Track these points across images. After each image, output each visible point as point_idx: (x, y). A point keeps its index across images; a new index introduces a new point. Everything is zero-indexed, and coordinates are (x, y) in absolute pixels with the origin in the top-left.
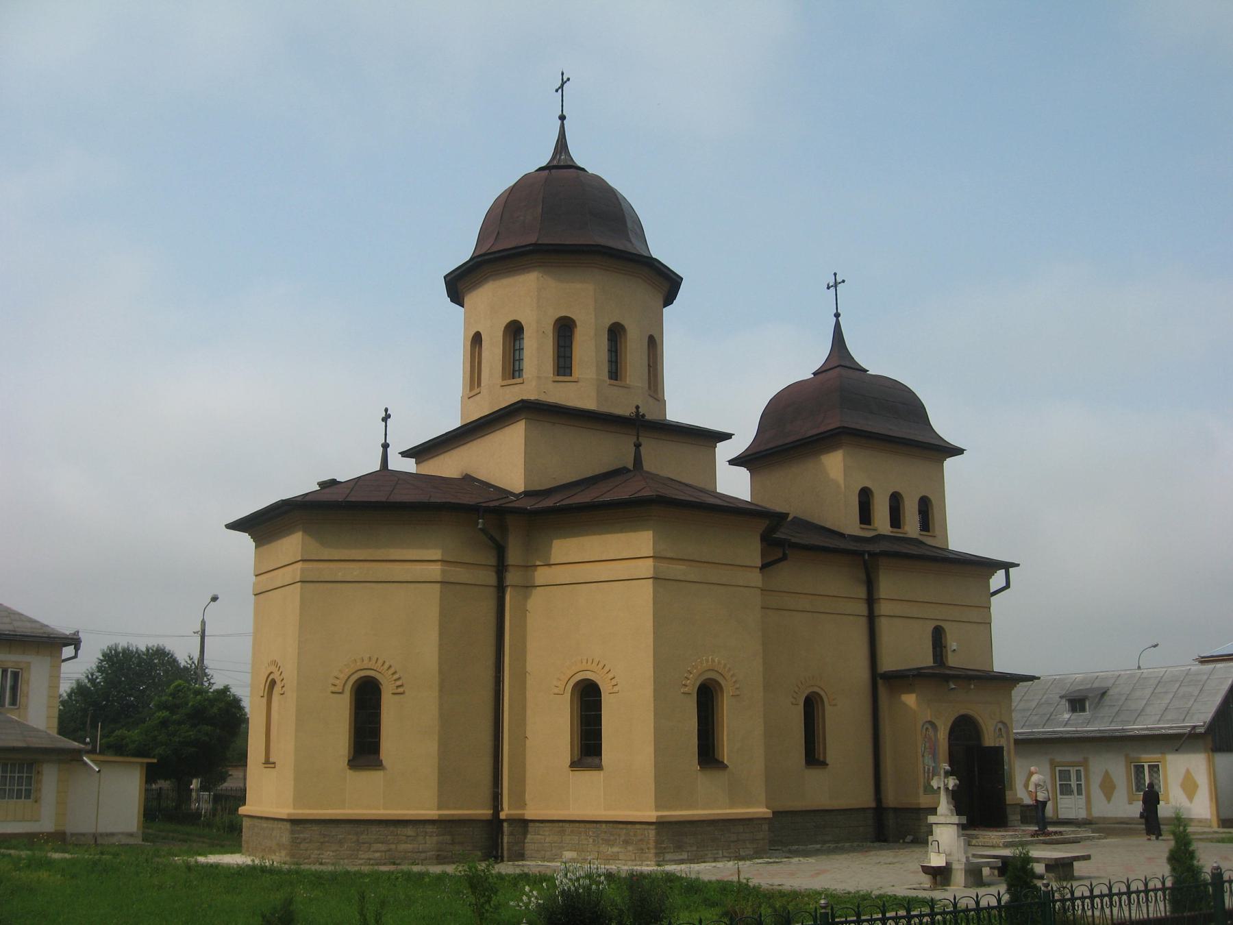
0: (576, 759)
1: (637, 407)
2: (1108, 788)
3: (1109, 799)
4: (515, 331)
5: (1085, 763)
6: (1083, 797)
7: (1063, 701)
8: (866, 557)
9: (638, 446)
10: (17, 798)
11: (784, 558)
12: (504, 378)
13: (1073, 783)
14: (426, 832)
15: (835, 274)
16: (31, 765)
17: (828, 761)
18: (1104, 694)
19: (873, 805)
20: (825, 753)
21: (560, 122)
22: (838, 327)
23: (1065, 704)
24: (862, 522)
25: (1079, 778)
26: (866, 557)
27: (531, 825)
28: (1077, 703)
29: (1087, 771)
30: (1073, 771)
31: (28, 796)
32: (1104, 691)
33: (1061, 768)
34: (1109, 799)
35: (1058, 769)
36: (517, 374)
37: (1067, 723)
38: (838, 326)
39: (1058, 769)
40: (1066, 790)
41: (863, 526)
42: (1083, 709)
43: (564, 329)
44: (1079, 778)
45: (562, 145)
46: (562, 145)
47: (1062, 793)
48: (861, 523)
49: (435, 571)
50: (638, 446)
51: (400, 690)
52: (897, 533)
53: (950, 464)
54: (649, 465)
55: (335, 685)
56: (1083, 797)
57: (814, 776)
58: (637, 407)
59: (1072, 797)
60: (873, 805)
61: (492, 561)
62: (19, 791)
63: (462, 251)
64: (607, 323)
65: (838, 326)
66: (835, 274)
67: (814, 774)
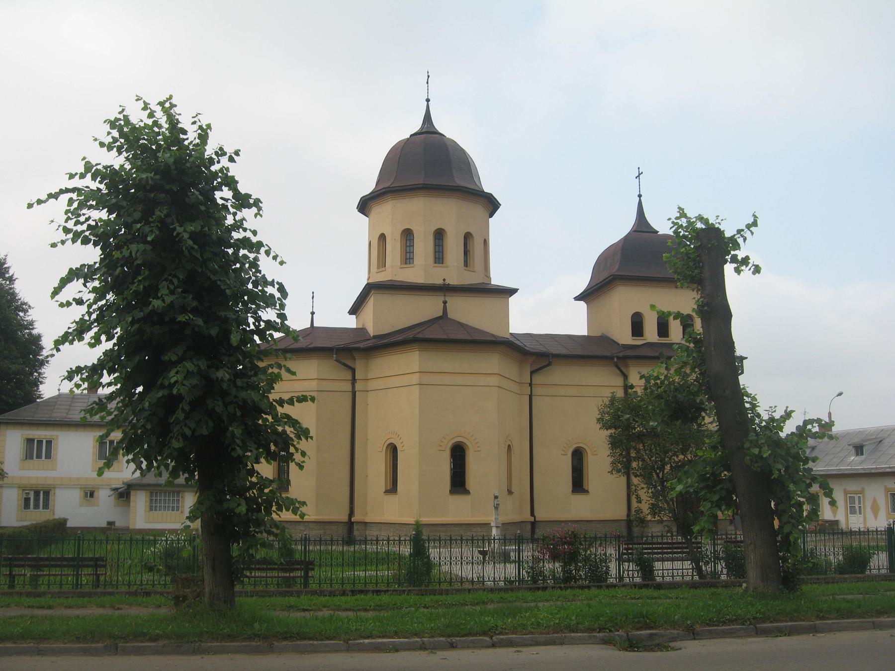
0: (389, 488)
1: (444, 280)
2: (875, 510)
3: (876, 517)
4: (408, 234)
5: (862, 492)
6: (862, 515)
7: (851, 447)
8: (615, 360)
9: (445, 303)
10: (177, 510)
11: (549, 364)
12: (401, 264)
13: (857, 506)
14: (309, 528)
15: (639, 168)
16: (178, 493)
17: (513, 491)
18: (880, 441)
19: (625, 518)
20: (588, 488)
21: (426, 103)
22: (640, 204)
23: (853, 451)
24: (633, 335)
25: (860, 503)
26: (615, 360)
27: (368, 524)
28: (859, 449)
29: (863, 497)
30: (856, 497)
31: (178, 510)
32: (879, 440)
33: (851, 495)
34: (876, 517)
35: (848, 495)
36: (408, 261)
37: (854, 462)
38: (640, 204)
39: (848, 495)
40: (853, 511)
41: (634, 338)
42: (862, 454)
43: (439, 235)
44: (860, 503)
45: (428, 118)
46: (428, 118)
47: (851, 513)
48: (633, 336)
49: (415, 379)
50: (445, 303)
51: (479, 449)
52: (664, 340)
53: (512, 300)
54: (451, 315)
55: (441, 446)
56: (862, 515)
57: (579, 499)
58: (444, 280)
59: (856, 515)
60: (625, 518)
61: (350, 377)
62: (173, 507)
63: (369, 186)
64: (433, 228)
65: (640, 204)
66: (639, 168)
67: (579, 498)
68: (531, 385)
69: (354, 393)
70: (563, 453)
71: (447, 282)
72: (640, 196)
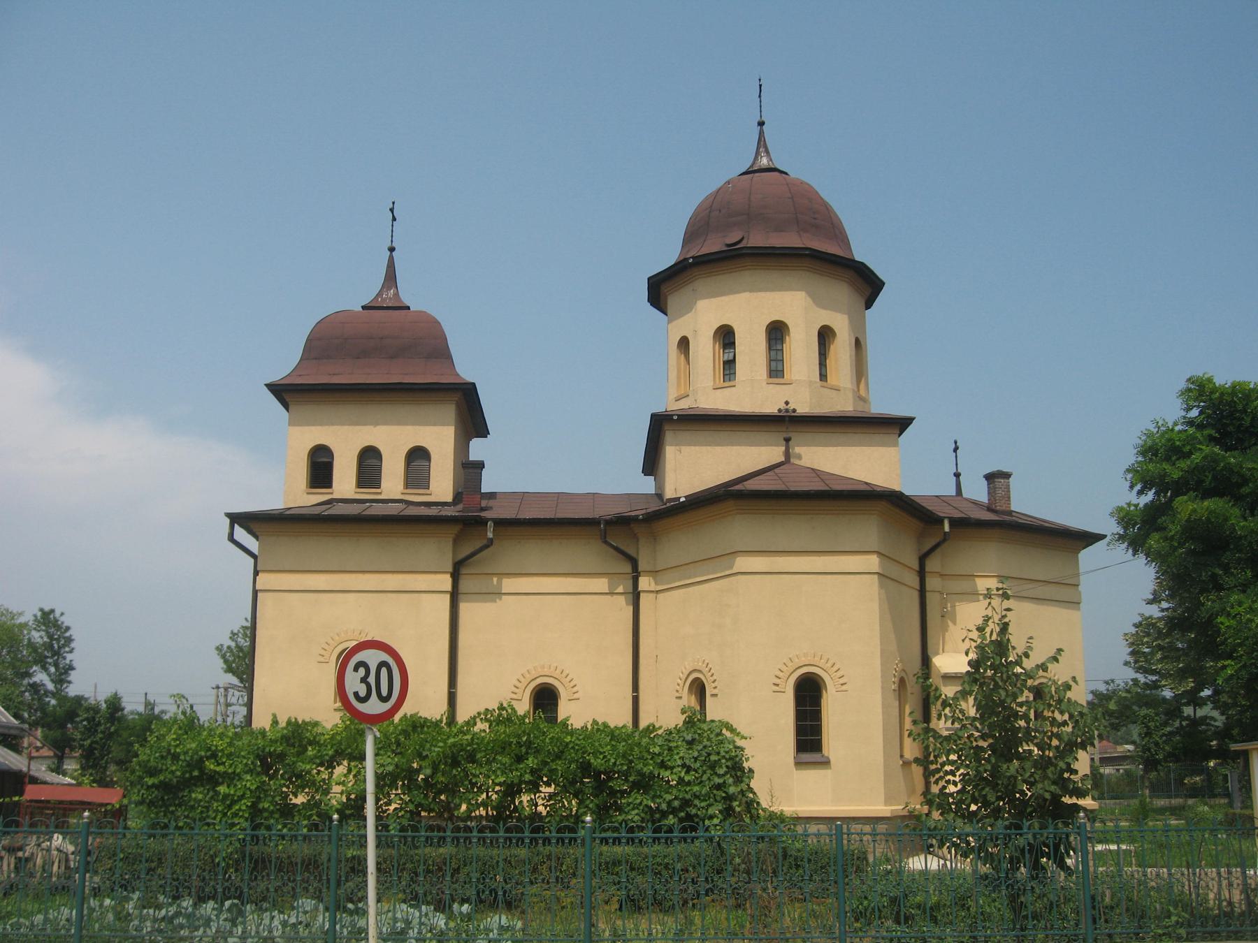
1: (787, 403)
52: (366, 494)
68: (922, 573)
70: (322, 659)
71: (791, 406)
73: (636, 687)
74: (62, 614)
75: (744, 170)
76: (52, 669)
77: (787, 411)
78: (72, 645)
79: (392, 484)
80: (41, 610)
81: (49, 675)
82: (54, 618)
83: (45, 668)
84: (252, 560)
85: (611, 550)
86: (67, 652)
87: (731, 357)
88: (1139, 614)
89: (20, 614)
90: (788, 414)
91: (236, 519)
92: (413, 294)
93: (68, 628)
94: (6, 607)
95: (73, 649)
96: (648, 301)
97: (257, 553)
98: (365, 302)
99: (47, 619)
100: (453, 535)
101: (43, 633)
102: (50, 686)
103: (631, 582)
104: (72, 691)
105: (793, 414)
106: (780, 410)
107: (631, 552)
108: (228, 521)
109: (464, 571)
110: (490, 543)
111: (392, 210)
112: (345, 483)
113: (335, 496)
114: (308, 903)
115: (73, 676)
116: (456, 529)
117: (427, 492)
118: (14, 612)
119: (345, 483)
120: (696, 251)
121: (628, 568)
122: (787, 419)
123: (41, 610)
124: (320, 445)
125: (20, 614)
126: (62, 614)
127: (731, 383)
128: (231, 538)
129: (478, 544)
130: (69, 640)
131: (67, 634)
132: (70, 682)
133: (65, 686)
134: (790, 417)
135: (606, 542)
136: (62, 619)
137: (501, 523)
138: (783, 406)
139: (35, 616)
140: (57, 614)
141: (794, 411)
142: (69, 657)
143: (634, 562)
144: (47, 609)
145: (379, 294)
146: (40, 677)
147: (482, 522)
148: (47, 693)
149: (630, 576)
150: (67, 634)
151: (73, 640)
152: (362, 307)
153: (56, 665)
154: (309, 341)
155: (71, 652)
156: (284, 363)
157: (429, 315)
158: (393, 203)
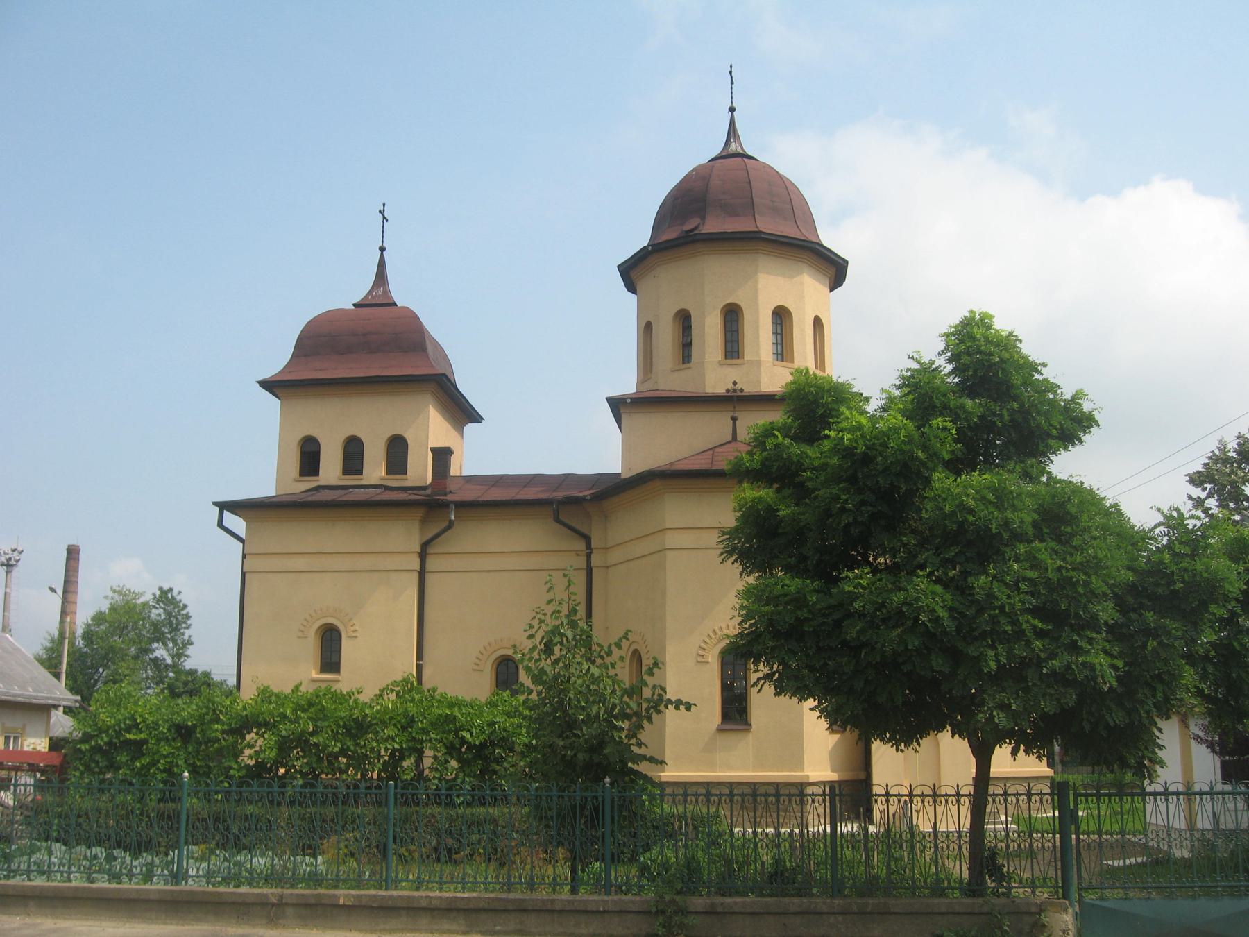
1: (735, 383)
9: (734, 419)
36: (686, 359)
43: (684, 320)
50: (734, 419)
52: (394, 482)
69: (589, 571)
71: (739, 386)
72: (382, 249)
73: (420, 656)
74: (180, 593)
75: (713, 156)
76: (171, 645)
77: (735, 391)
78: (189, 622)
79: (375, 470)
80: (160, 589)
81: (168, 650)
82: (172, 596)
83: (165, 645)
84: (241, 545)
85: (566, 530)
86: (185, 628)
87: (689, 341)
88: (145, 592)
89: (142, 594)
90: (736, 394)
91: (223, 506)
92: (401, 294)
93: (185, 606)
94: (128, 587)
95: (190, 625)
96: (629, 290)
97: (244, 538)
98: (357, 299)
99: (165, 597)
100: (419, 518)
101: (161, 611)
102: (169, 661)
103: (585, 558)
104: (189, 664)
105: (740, 394)
106: (728, 391)
107: (584, 530)
108: (217, 509)
109: (430, 550)
110: (450, 526)
111: (382, 212)
112: (331, 470)
113: (322, 483)
114: (145, 855)
115: (190, 650)
116: (421, 512)
117: (404, 477)
118: (136, 592)
119: (331, 470)
120: (665, 237)
121: (581, 545)
122: (735, 399)
123: (160, 589)
124: (353, 436)
125: (142, 594)
126: (180, 593)
127: (687, 365)
128: (220, 524)
129: (444, 525)
130: (188, 617)
131: (184, 612)
132: (188, 656)
133: (182, 660)
134: (738, 396)
135: (558, 521)
136: (178, 598)
137: (462, 506)
138: (730, 386)
139: (154, 594)
140: (175, 592)
141: (742, 390)
142: (188, 633)
143: (587, 539)
144: (165, 588)
145: (370, 292)
146: (160, 652)
147: (444, 505)
148: (167, 666)
149: (585, 553)
150: (184, 612)
151: (190, 617)
152: (354, 305)
153: (175, 641)
154: (300, 339)
155: (187, 628)
156: (276, 360)
157: (412, 312)
158: (384, 205)
